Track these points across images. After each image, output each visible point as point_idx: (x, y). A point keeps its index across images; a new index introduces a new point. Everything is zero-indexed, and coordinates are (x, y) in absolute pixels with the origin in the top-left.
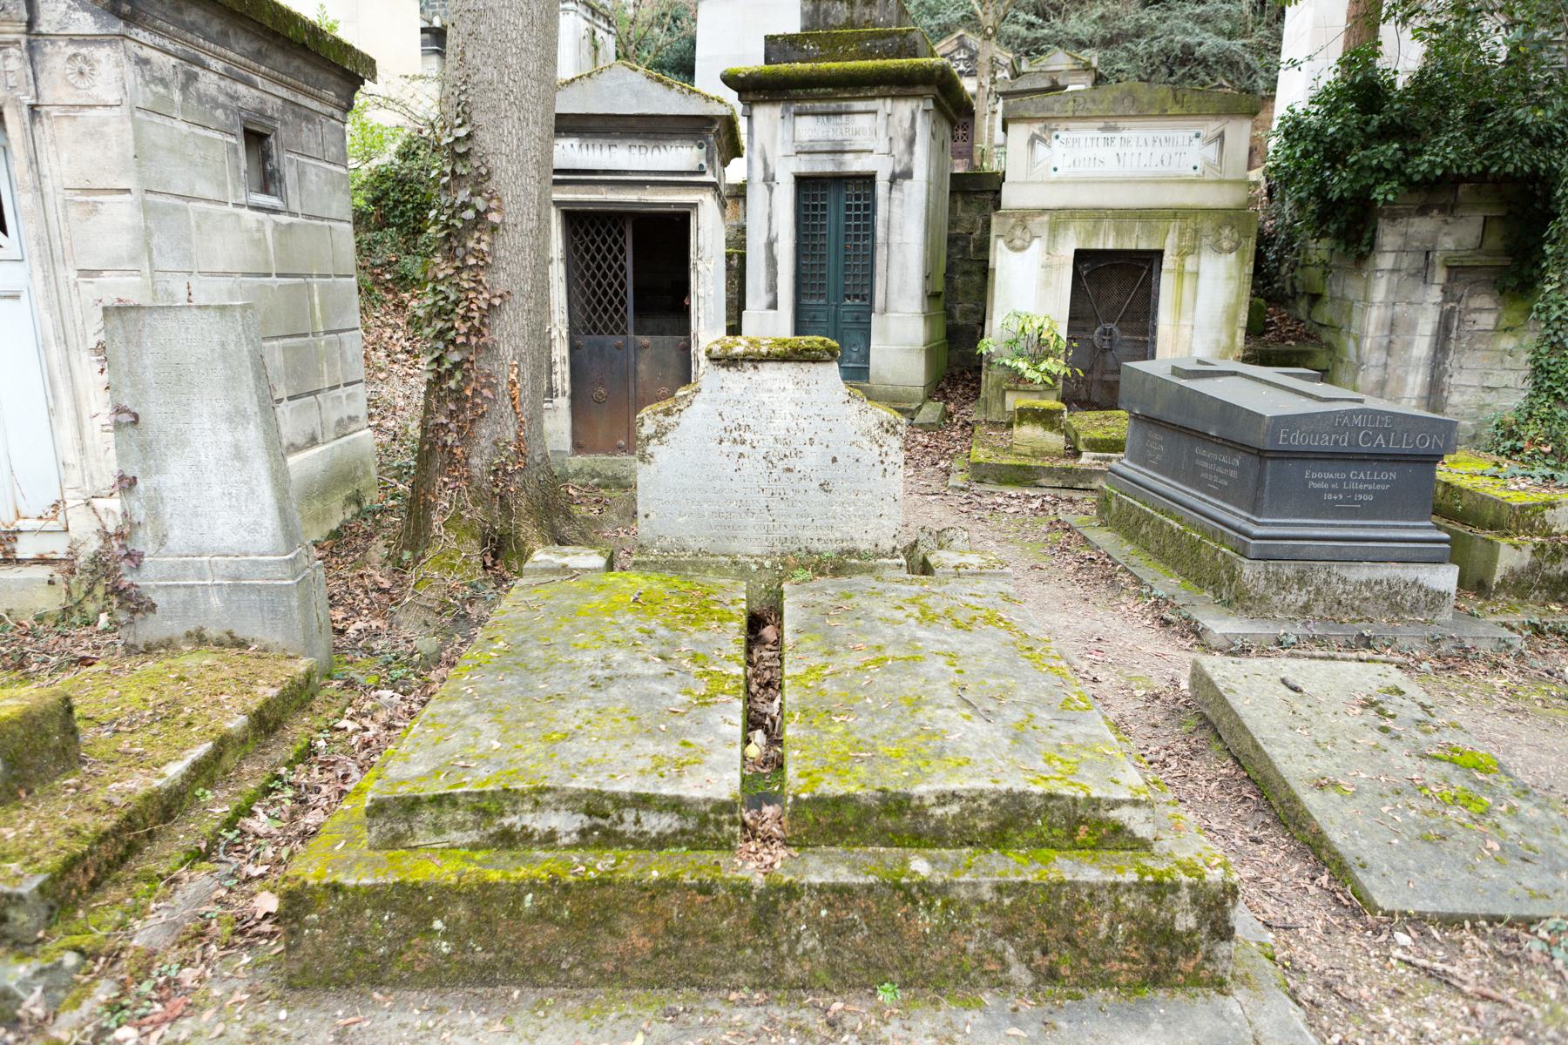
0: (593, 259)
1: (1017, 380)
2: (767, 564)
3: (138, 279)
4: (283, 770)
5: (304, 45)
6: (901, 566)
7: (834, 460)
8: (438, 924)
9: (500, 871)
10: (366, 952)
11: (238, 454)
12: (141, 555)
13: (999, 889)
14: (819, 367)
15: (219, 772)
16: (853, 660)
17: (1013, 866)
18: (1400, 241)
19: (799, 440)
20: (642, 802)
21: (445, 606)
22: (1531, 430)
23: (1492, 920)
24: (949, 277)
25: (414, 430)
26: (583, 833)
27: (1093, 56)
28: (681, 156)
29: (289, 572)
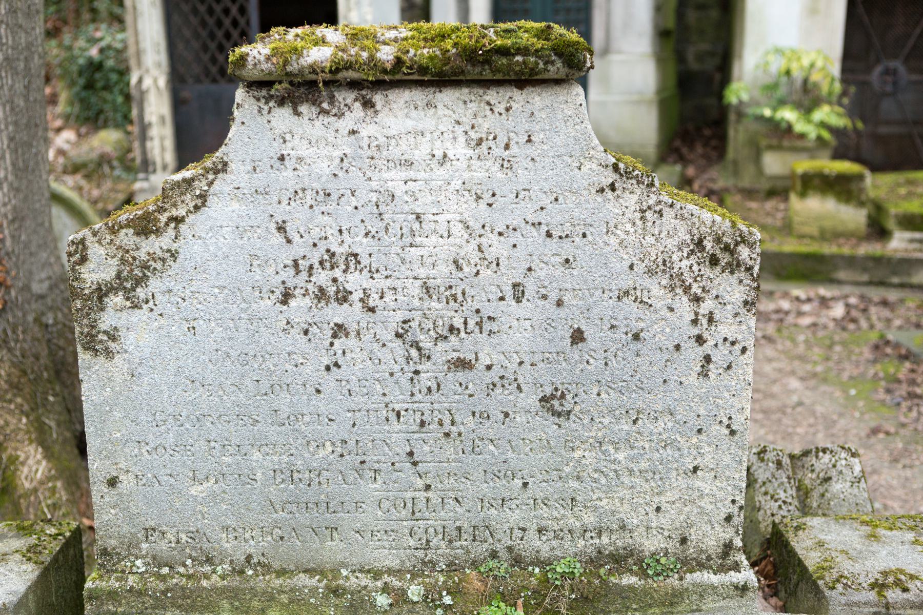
1: (782, 135)
2: (415, 592)
6: (743, 589)
7: (578, 337)
19: (485, 289)
24: (680, 14)
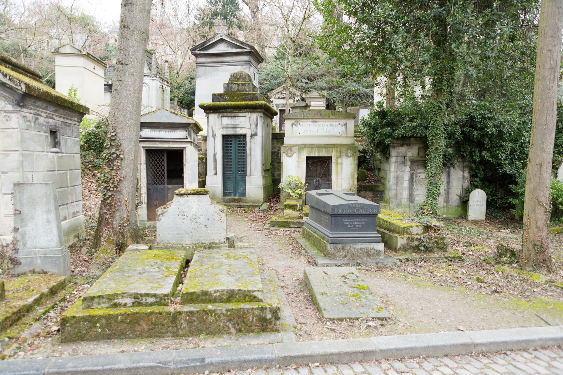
0: (155, 163)
1: (289, 197)
3: (19, 174)
4: (58, 303)
5: (69, 107)
8: (98, 325)
9: (113, 312)
10: (80, 332)
11: (48, 221)
12: (18, 249)
13: (227, 310)
14: (203, 196)
15: (41, 303)
16: (206, 267)
17: (232, 306)
18: (396, 154)
20: (147, 295)
21: (104, 263)
22: (427, 207)
23: (350, 319)
25: (97, 215)
26: (133, 303)
27: (325, 93)
28: (181, 134)
29: (61, 252)
